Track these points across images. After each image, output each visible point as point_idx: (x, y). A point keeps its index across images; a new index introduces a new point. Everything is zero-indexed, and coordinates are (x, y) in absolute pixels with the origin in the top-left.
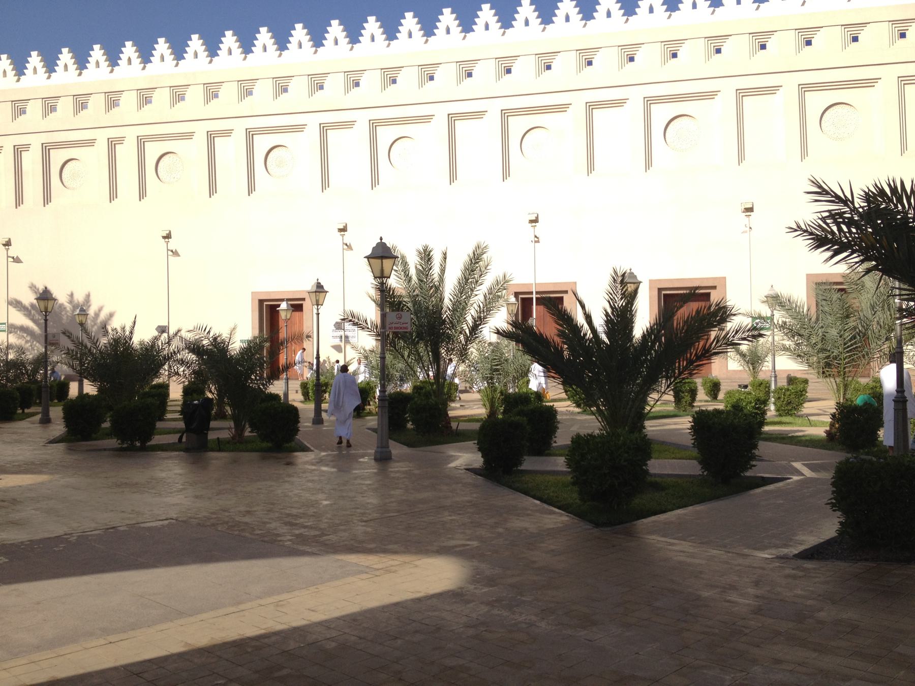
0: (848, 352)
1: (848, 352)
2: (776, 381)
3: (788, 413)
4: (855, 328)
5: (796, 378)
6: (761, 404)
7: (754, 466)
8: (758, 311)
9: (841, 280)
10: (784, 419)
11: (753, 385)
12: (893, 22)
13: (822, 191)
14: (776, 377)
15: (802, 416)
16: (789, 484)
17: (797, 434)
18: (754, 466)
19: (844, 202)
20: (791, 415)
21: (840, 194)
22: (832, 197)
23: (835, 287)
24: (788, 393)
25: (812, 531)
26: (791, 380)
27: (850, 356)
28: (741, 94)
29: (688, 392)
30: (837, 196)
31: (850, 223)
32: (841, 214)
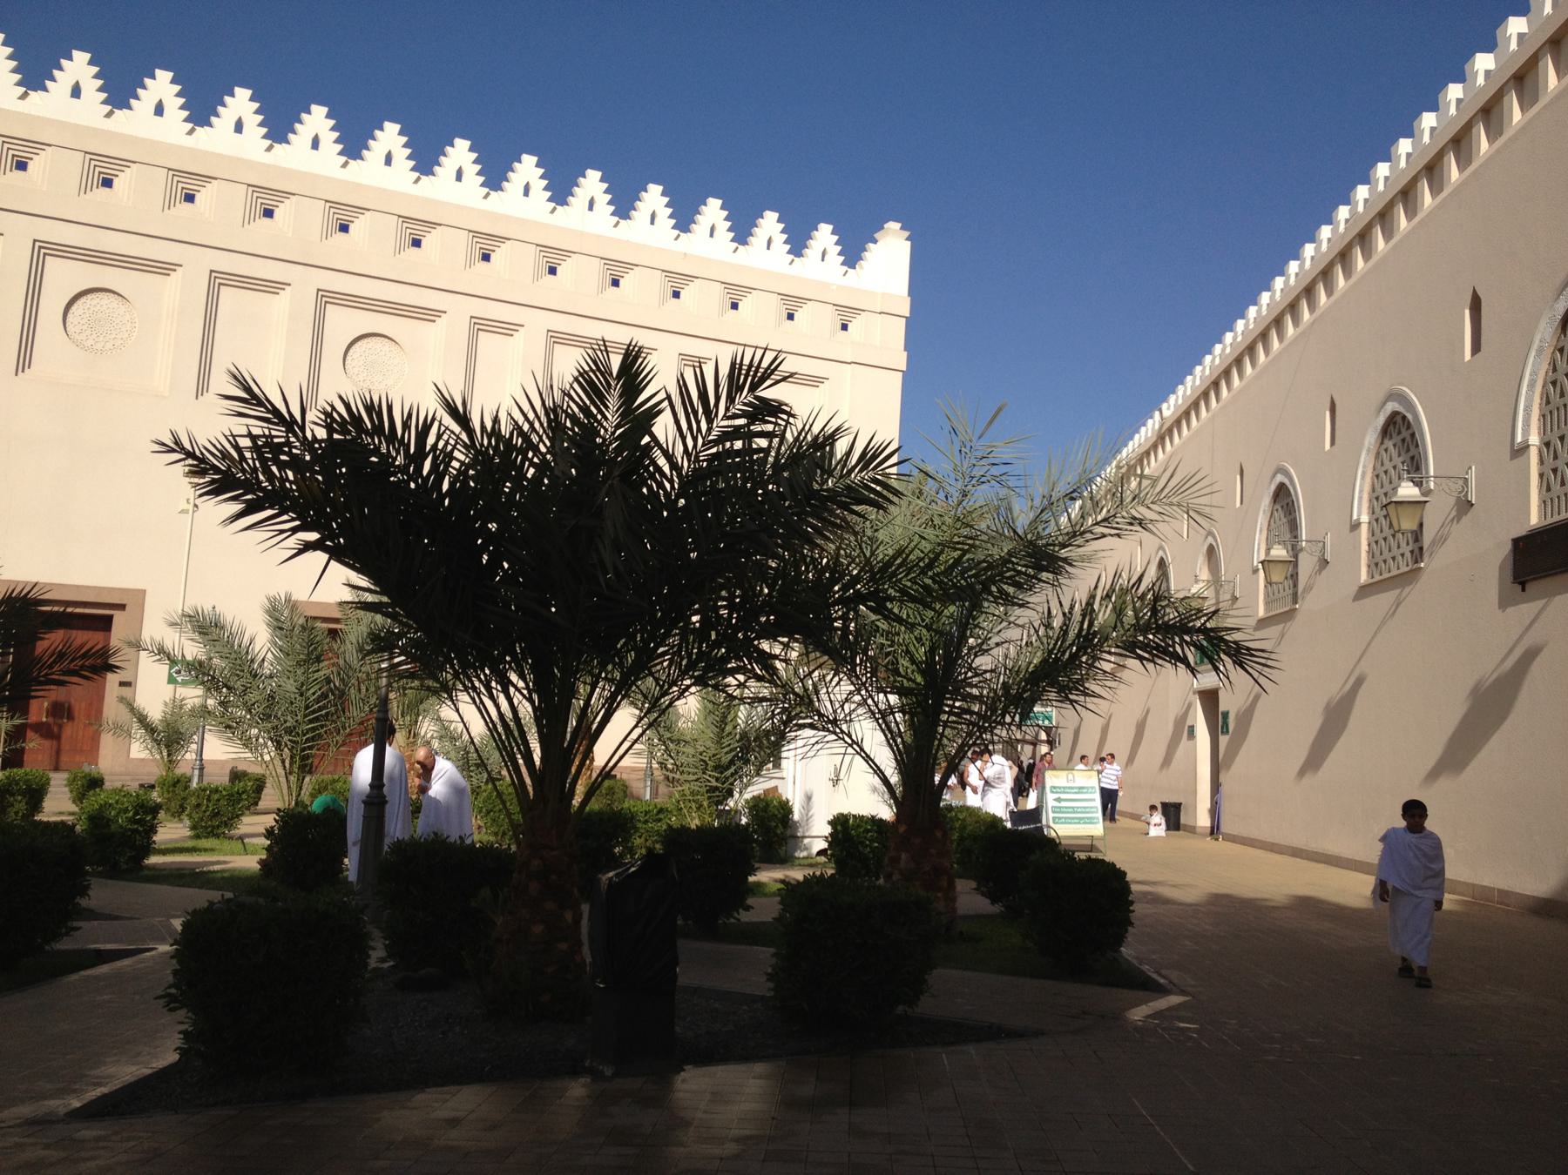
0: (311, 721)
1: (311, 721)
2: (201, 776)
3: (213, 833)
4: (328, 681)
5: (245, 774)
6: (146, 813)
7: (77, 929)
8: (158, 638)
9: (337, 615)
10: (204, 843)
11: (162, 783)
12: (476, 233)
13: (251, 397)
14: (202, 769)
15: (231, 838)
16: (143, 961)
17: (211, 868)
18: (77, 929)
19: (289, 424)
20: (217, 836)
21: (284, 411)
22: (268, 411)
23: (325, 625)
24: (216, 796)
25: (138, 1054)
26: (236, 776)
27: (313, 729)
28: (218, 281)
29: (23, 793)
30: (276, 412)
31: (295, 463)
32: (277, 449)
